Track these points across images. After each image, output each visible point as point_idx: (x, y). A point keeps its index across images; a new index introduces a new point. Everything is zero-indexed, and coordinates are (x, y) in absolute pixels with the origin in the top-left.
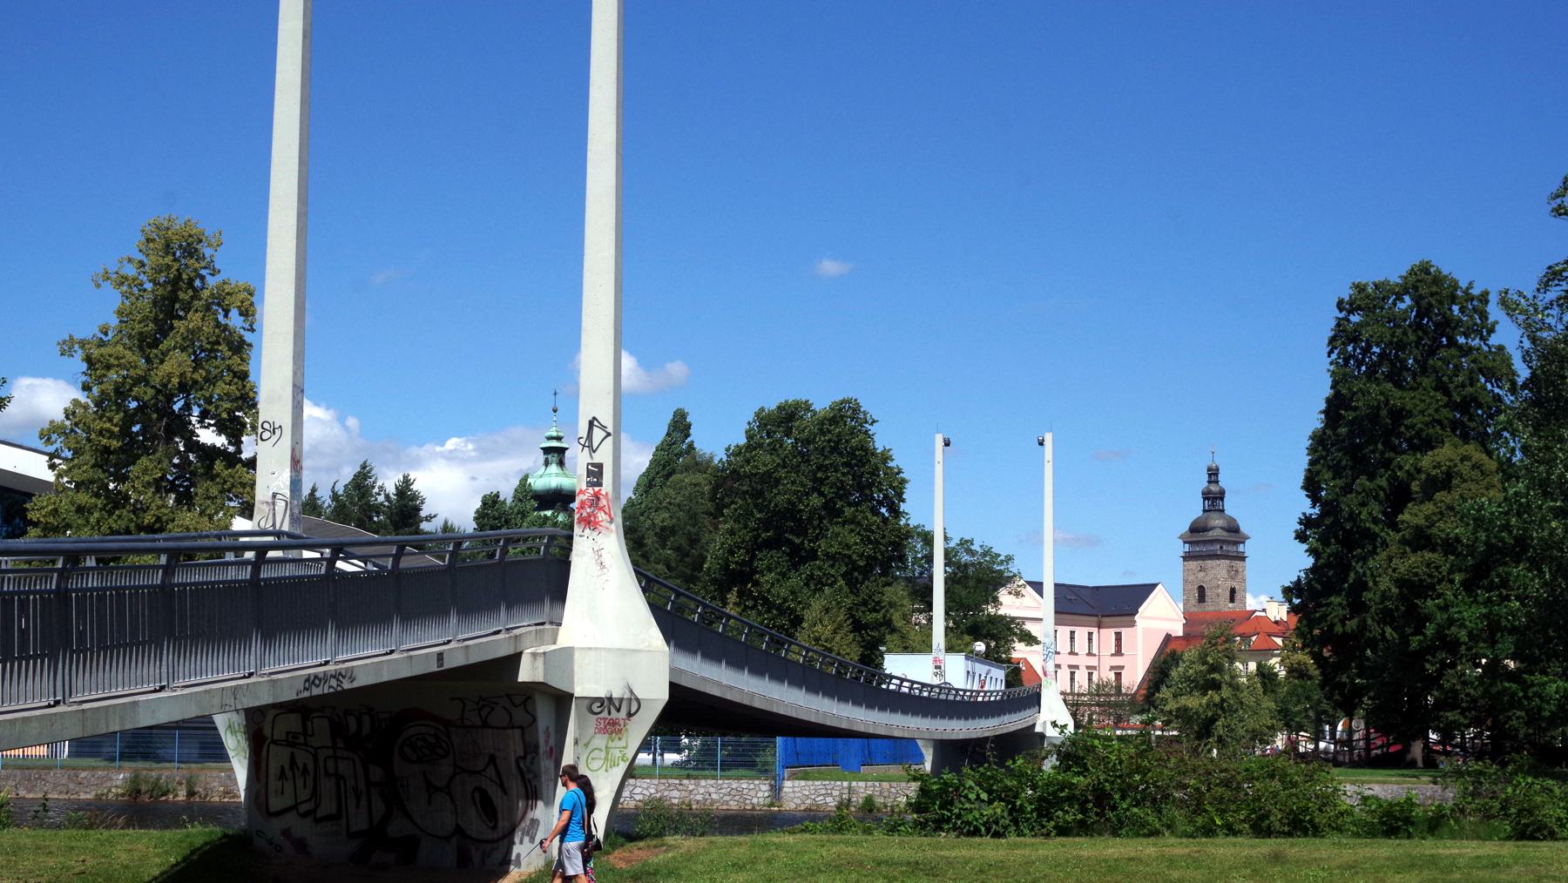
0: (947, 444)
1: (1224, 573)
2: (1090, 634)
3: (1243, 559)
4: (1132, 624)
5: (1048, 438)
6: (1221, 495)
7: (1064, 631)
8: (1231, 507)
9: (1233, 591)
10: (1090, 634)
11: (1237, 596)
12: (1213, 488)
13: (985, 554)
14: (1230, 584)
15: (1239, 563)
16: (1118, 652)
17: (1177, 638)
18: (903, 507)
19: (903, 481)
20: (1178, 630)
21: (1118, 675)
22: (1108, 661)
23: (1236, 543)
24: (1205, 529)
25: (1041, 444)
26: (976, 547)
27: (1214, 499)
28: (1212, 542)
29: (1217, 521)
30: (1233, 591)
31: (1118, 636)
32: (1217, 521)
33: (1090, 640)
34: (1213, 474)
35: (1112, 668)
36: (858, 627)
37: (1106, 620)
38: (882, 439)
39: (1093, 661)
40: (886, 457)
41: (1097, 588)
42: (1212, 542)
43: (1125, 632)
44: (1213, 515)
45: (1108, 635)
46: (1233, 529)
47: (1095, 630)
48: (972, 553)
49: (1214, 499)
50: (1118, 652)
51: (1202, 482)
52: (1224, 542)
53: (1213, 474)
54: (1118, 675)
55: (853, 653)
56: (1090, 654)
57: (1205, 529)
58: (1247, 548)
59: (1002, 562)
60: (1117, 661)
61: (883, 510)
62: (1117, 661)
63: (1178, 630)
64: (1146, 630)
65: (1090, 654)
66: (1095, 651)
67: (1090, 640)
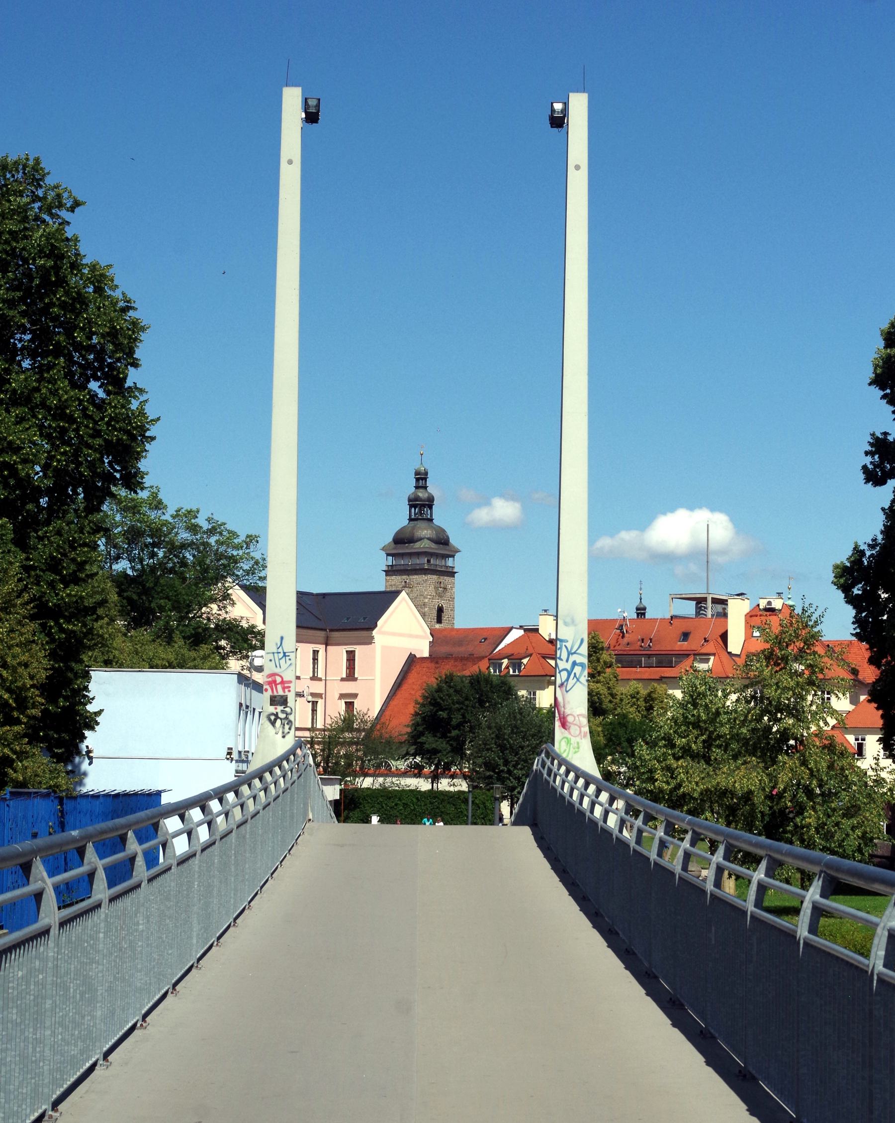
0: (311, 117)
1: (431, 590)
2: (316, 652)
3: (452, 574)
4: (369, 641)
5: (578, 107)
6: (429, 503)
7: (307, 649)
8: (440, 516)
9: (440, 610)
10: (316, 652)
11: (445, 617)
12: (421, 494)
13: (212, 531)
14: (437, 602)
15: (446, 579)
16: (351, 676)
17: (423, 659)
18: (133, 377)
19: (135, 325)
20: (423, 650)
21: (350, 705)
22: (337, 688)
23: (445, 557)
24: (412, 540)
25: (558, 122)
27: (421, 506)
28: (418, 554)
29: (424, 532)
30: (440, 610)
31: (351, 656)
32: (424, 532)
33: (315, 660)
34: (421, 478)
35: (342, 696)
36: (43, 612)
37: (336, 634)
38: (94, 238)
40: (100, 280)
41: (324, 595)
42: (418, 554)
43: (359, 650)
44: (420, 524)
45: (338, 654)
46: (442, 540)
47: (321, 648)
48: (194, 529)
49: (421, 506)
50: (351, 676)
51: (409, 487)
52: (432, 555)
53: (421, 478)
54: (350, 705)
55: (40, 666)
56: (314, 678)
57: (412, 540)
58: (456, 563)
59: (238, 547)
60: (349, 687)
61: (94, 385)
62: (349, 687)
63: (423, 650)
64: (384, 648)
65: (314, 678)
66: (321, 674)
67: (315, 660)
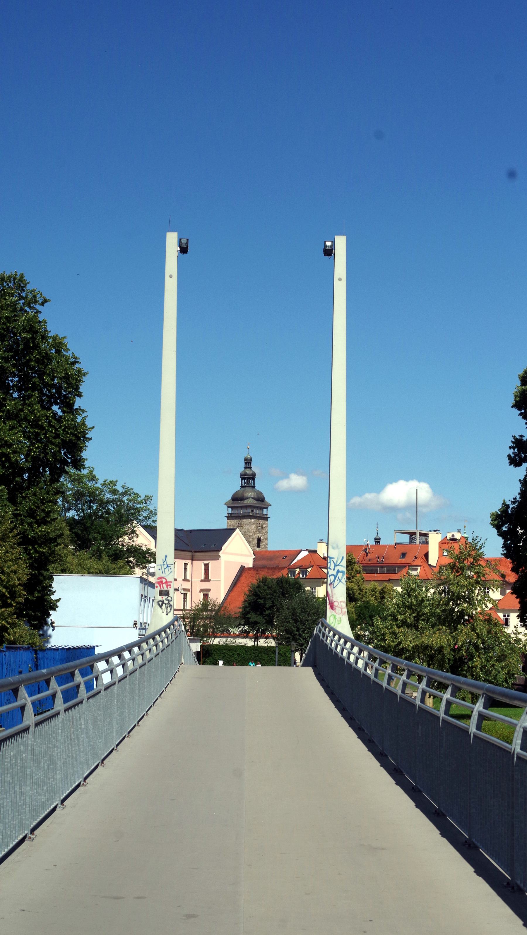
0: (183, 250)
2: (186, 565)
3: (266, 519)
4: (217, 558)
5: (341, 244)
6: (253, 477)
8: (259, 484)
9: (259, 540)
10: (186, 565)
11: (262, 544)
12: (248, 471)
13: (125, 494)
14: (257, 535)
16: (206, 578)
18: (78, 403)
19: (80, 373)
20: (249, 564)
21: (206, 596)
22: (198, 585)
24: (242, 499)
25: (329, 253)
26: (119, 488)
27: (248, 478)
28: (246, 507)
29: (250, 494)
30: (259, 540)
31: (207, 567)
32: (250, 494)
33: (186, 569)
34: (248, 462)
35: (201, 590)
36: (25, 541)
38: (56, 321)
39: (187, 585)
40: (59, 345)
41: (191, 531)
42: (246, 507)
43: (212, 563)
44: (247, 489)
45: (199, 565)
46: (260, 499)
47: (189, 562)
48: (114, 492)
49: (248, 478)
50: (206, 578)
51: (241, 468)
53: (248, 462)
54: (206, 596)
55: (23, 573)
56: (185, 580)
57: (242, 499)
58: (269, 512)
59: (140, 503)
60: (206, 585)
61: (55, 408)
62: (206, 585)
63: (249, 564)
65: (185, 580)
66: (189, 578)
67: (186, 569)
